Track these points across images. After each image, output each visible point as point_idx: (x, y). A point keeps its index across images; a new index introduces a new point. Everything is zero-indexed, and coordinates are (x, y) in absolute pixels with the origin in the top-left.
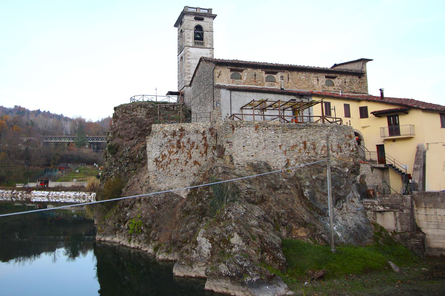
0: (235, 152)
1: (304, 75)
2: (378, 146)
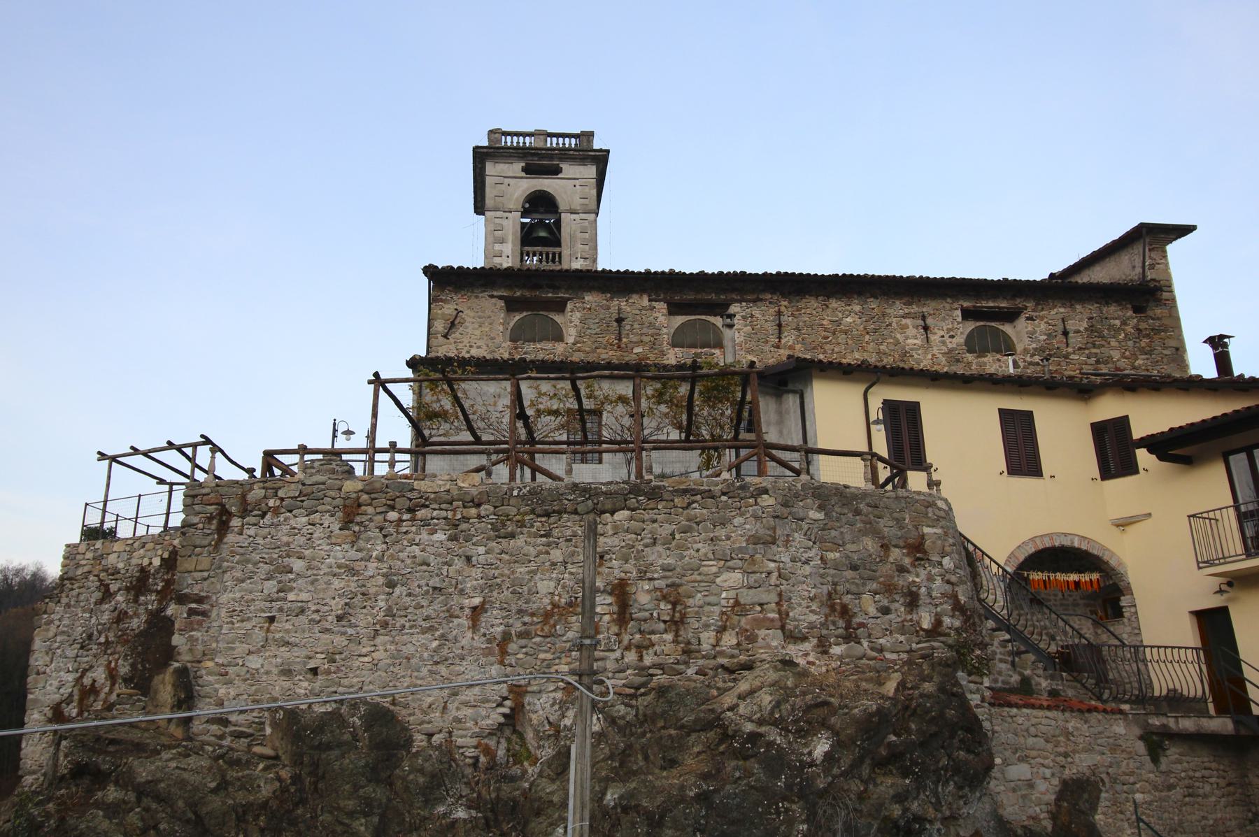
0: (215, 653)
1: (857, 308)
2: (1202, 617)
